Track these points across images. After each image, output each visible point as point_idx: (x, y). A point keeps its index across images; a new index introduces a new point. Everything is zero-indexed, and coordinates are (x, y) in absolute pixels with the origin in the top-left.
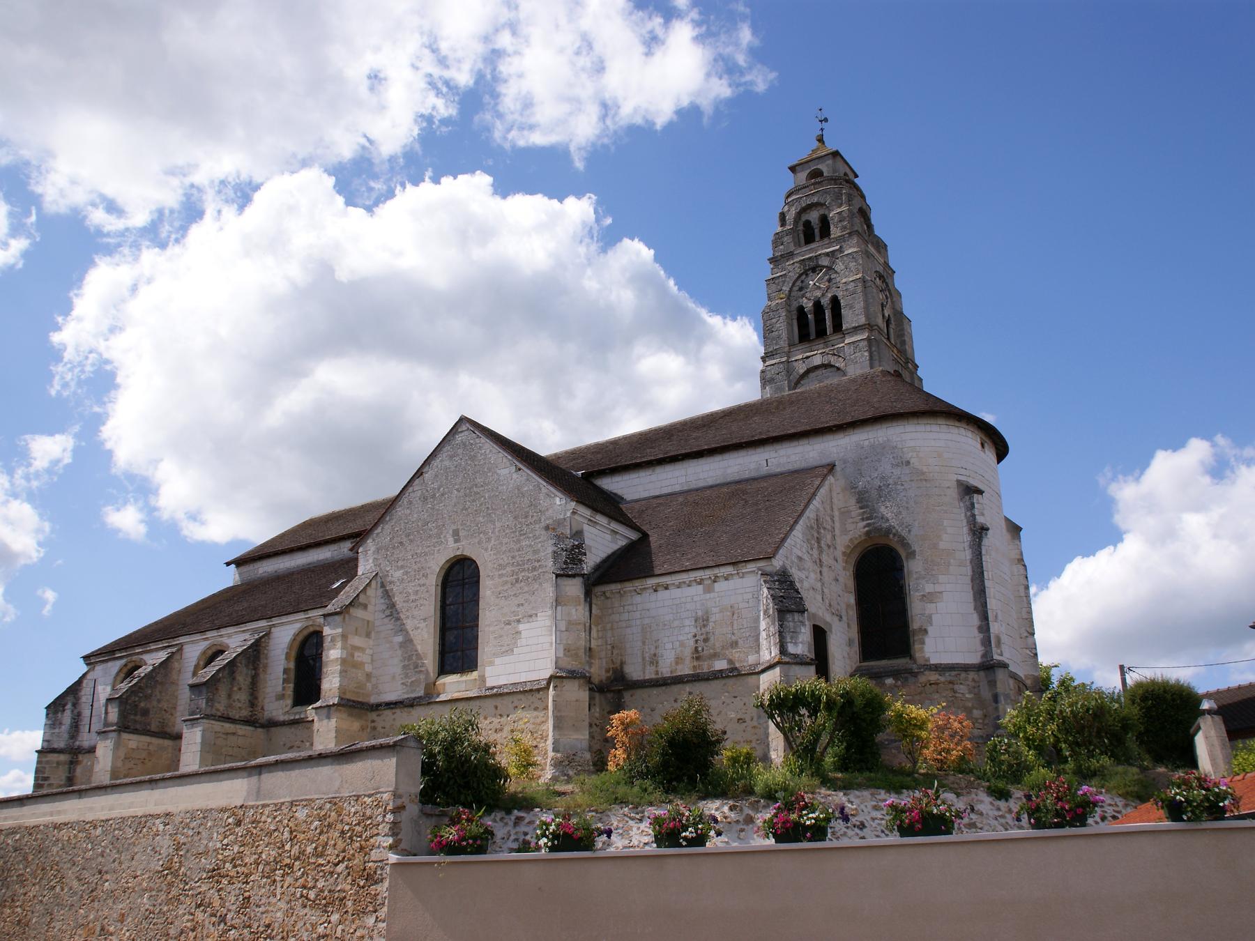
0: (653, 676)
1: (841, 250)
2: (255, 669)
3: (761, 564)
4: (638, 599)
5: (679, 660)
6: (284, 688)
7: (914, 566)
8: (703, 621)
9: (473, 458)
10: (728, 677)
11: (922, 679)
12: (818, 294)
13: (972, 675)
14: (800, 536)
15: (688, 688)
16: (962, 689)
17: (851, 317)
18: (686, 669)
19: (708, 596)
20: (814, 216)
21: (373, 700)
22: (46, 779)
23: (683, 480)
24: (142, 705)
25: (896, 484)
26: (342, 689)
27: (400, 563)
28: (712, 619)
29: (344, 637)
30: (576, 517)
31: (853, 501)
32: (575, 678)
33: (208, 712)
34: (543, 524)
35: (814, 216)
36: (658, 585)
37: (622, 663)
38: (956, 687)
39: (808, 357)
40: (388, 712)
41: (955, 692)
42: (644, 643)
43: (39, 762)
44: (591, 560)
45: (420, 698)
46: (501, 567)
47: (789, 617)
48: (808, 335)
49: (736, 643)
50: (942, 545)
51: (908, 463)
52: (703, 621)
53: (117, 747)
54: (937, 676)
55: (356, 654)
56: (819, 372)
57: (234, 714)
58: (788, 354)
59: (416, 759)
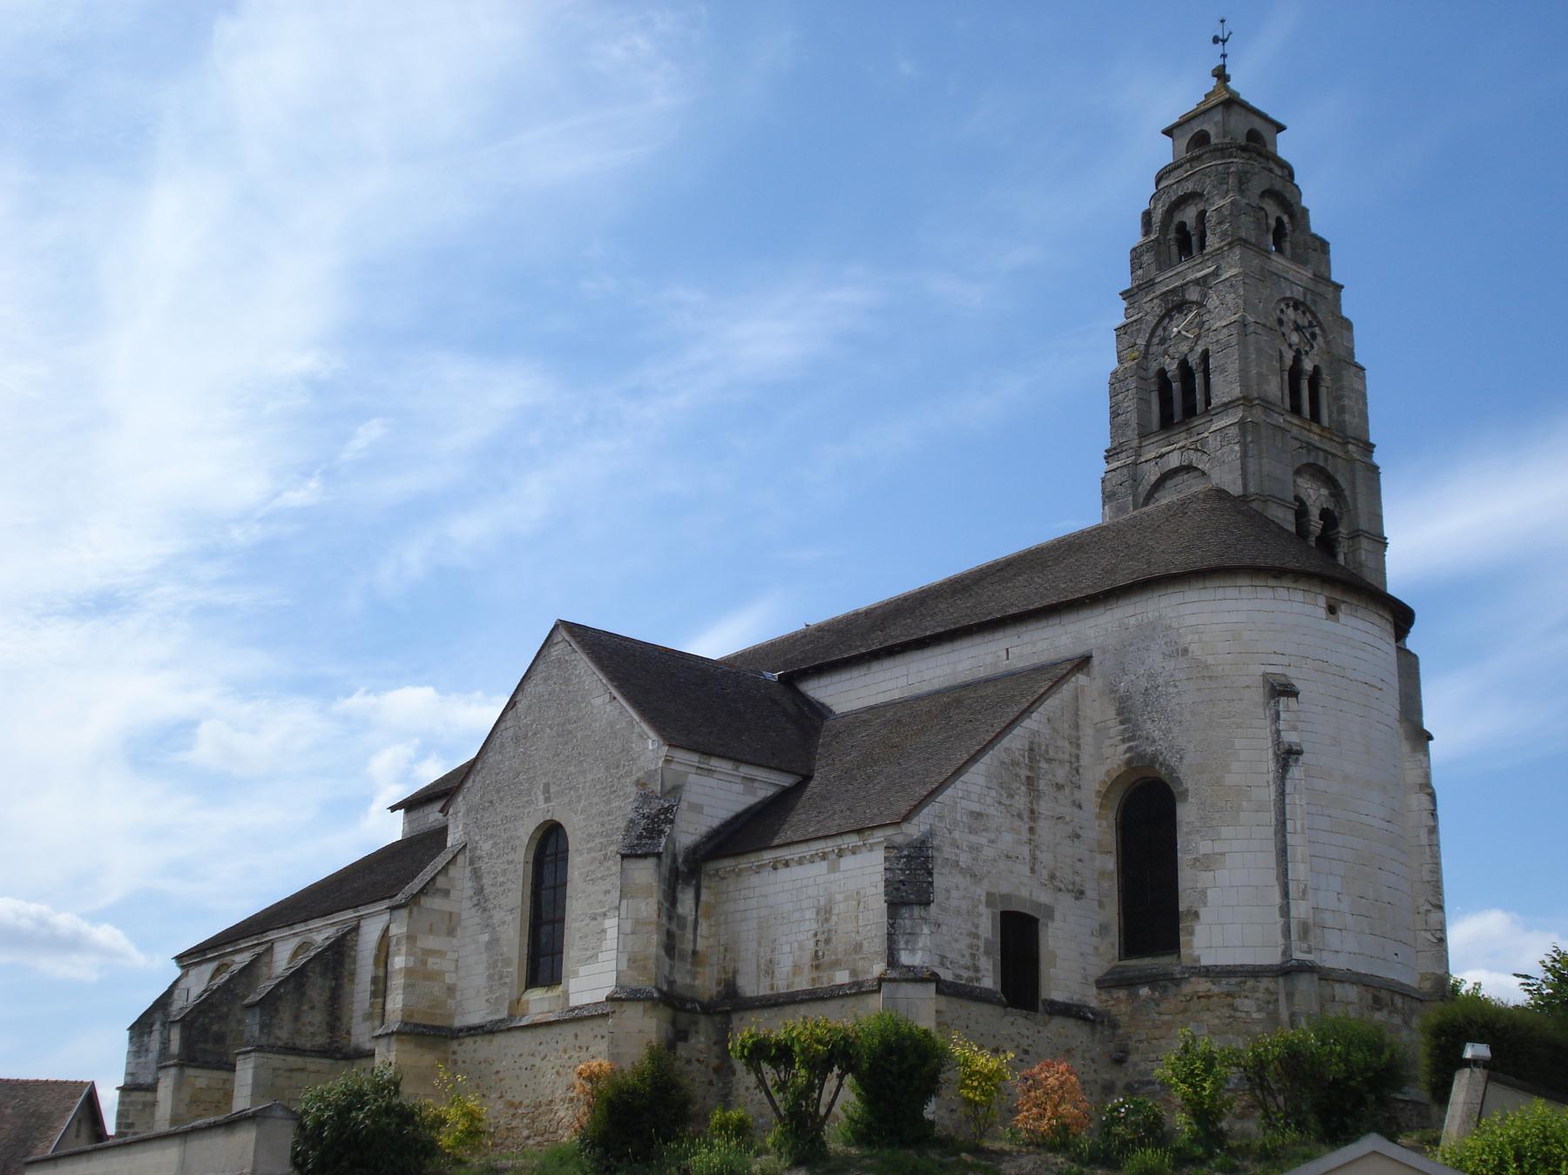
0: (768, 992)
1: (1215, 274)
2: (336, 979)
3: (889, 832)
4: (755, 880)
5: (797, 969)
6: (372, 1005)
7: (1186, 814)
9: (567, 681)
10: (846, 995)
11: (1187, 989)
12: (1184, 348)
13: (1265, 983)
14: (982, 781)
15: (803, 1010)
17: (1225, 387)
18: (803, 984)
19: (832, 876)
20: (1189, 215)
21: (458, 1022)
22: (130, 1125)
23: (903, 682)
24: (215, 1028)
25: (1167, 684)
26: (407, 1011)
27: (489, 831)
29: (411, 938)
30: (673, 766)
31: (1112, 713)
32: (639, 1000)
33: (264, 1041)
34: (634, 778)
37: (735, 972)
38: (1237, 1002)
39: (1161, 456)
40: (469, 1041)
41: (1235, 1009)
42: (759, 944)
43: (121, 1103)
44: (689, 830)
45: (502, 1021)
46: (591, 837)
47: (905, 912)
48: (1172, 416)
49: (861, 945)
50: (1230, 779)
51: (1186, 651)
52: (825, 913)
53: (178, 1087)
54: (1209, 985)
55: (430, 960)
56: (1179, 479)
57: (304, 1042)
58: (1138, 452)
59: (285, 1135)
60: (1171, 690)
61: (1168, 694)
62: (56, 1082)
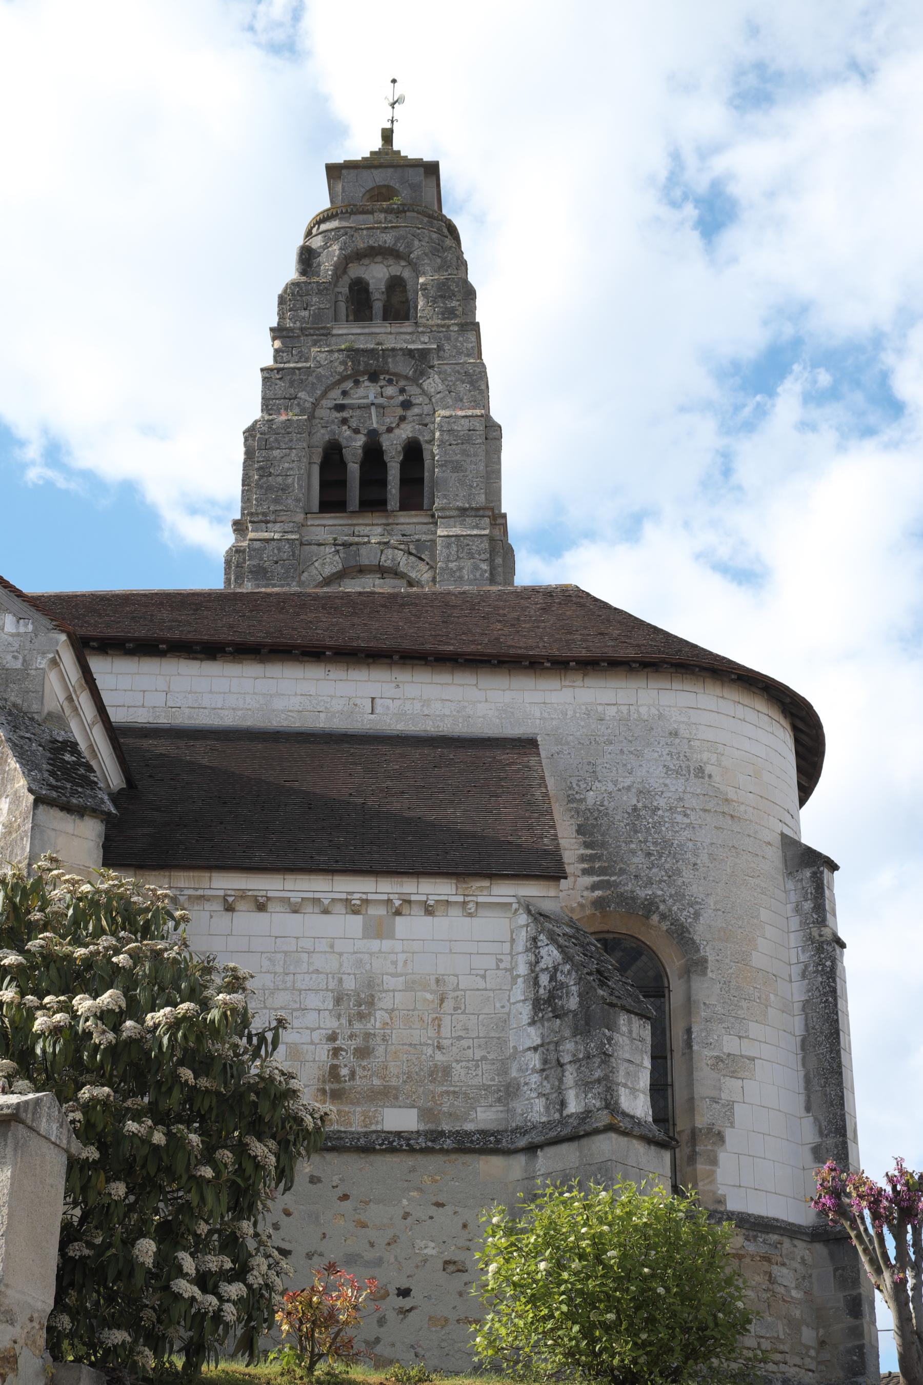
8: (359, 1003)
16: (785, 1275)
19: (375, 945)
20: (377, 274)
23: (158, 700)
28: (385, 1002)
35: (377, 274)
36: (242, 895)
38: (776, 1270)
50: (757, 960)
60: (679, 818)
61: (673, 823)
62: (616, 609)
